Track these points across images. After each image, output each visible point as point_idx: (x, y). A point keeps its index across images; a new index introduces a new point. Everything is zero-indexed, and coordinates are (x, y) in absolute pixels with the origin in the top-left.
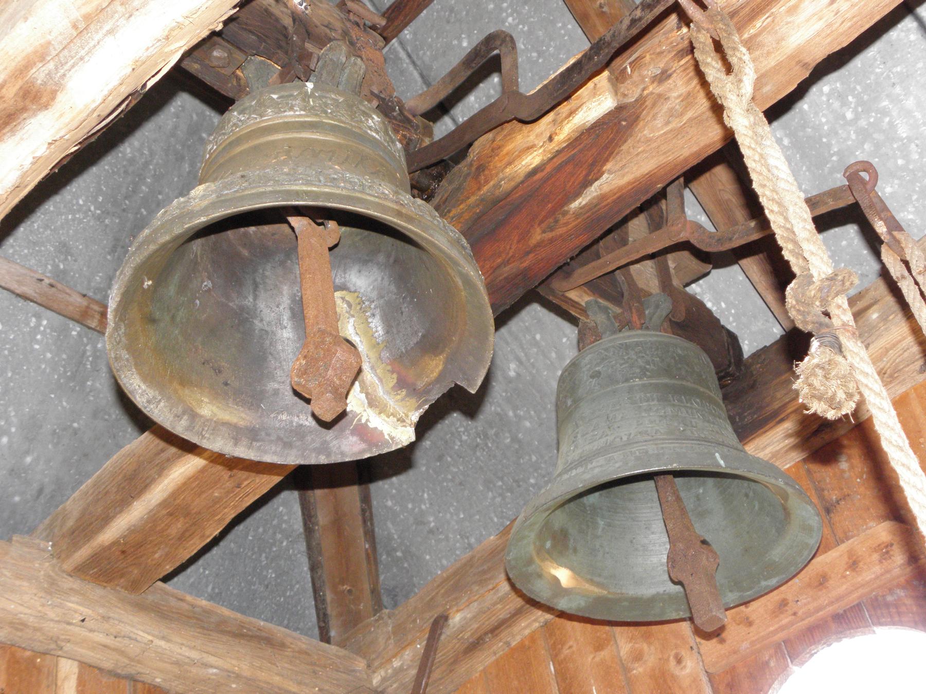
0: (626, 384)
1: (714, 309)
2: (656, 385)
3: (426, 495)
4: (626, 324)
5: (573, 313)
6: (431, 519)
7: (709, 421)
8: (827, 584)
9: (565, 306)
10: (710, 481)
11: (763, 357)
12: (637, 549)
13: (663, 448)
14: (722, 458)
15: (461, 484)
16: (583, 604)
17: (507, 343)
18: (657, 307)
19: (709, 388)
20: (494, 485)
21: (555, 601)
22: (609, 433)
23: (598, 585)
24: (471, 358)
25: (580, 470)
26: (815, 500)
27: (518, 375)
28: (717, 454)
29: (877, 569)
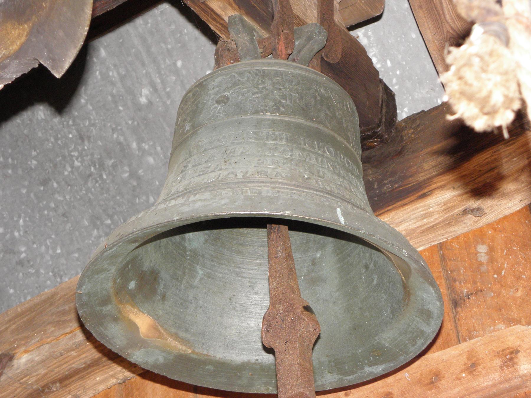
0: (255, 117)
1: (378, 66)
2: (289, 124)
3: (21, 221)
4: (270, 51)
5: (213, 28)
6: (23, 249)
7: (339, 175)
8: (439, 384)
9: (204, 18)
10: (330, 241)
11: (418, 122)
12: (235, 309)
13: (279, 192)
14: (343, 215)
15: (64, 215)
16: (161, 360)
17: (143, 65)
18: (309, 38)
19: (347, 139)
20: (102, 223)
21: (130, 351)
22: (224, 167)
23: (183, 341)
24: (61, 33)
25: (180, 201)
26: (444, 291)
27: (150, 103)
28: (338, 210)
29: (496, 376)
